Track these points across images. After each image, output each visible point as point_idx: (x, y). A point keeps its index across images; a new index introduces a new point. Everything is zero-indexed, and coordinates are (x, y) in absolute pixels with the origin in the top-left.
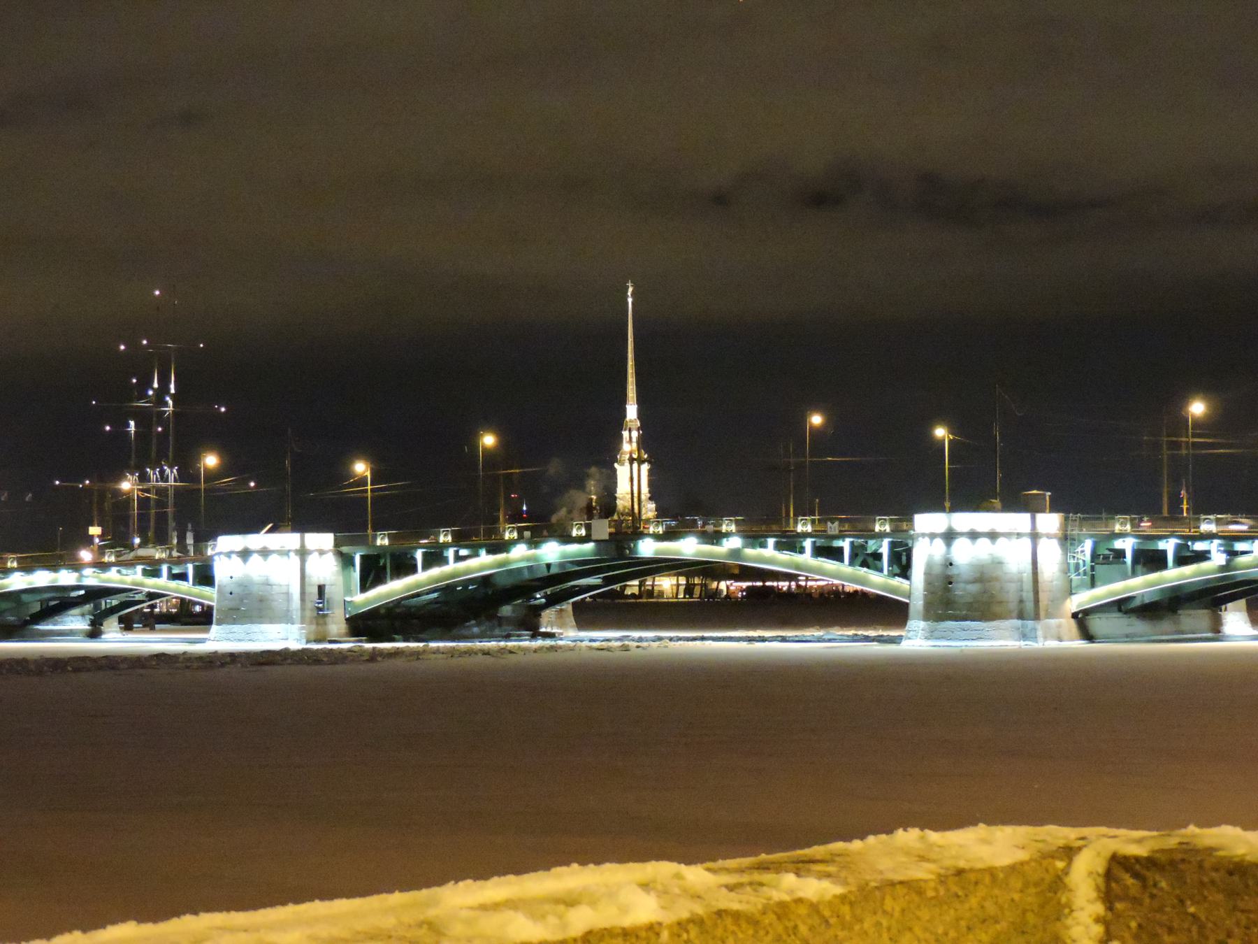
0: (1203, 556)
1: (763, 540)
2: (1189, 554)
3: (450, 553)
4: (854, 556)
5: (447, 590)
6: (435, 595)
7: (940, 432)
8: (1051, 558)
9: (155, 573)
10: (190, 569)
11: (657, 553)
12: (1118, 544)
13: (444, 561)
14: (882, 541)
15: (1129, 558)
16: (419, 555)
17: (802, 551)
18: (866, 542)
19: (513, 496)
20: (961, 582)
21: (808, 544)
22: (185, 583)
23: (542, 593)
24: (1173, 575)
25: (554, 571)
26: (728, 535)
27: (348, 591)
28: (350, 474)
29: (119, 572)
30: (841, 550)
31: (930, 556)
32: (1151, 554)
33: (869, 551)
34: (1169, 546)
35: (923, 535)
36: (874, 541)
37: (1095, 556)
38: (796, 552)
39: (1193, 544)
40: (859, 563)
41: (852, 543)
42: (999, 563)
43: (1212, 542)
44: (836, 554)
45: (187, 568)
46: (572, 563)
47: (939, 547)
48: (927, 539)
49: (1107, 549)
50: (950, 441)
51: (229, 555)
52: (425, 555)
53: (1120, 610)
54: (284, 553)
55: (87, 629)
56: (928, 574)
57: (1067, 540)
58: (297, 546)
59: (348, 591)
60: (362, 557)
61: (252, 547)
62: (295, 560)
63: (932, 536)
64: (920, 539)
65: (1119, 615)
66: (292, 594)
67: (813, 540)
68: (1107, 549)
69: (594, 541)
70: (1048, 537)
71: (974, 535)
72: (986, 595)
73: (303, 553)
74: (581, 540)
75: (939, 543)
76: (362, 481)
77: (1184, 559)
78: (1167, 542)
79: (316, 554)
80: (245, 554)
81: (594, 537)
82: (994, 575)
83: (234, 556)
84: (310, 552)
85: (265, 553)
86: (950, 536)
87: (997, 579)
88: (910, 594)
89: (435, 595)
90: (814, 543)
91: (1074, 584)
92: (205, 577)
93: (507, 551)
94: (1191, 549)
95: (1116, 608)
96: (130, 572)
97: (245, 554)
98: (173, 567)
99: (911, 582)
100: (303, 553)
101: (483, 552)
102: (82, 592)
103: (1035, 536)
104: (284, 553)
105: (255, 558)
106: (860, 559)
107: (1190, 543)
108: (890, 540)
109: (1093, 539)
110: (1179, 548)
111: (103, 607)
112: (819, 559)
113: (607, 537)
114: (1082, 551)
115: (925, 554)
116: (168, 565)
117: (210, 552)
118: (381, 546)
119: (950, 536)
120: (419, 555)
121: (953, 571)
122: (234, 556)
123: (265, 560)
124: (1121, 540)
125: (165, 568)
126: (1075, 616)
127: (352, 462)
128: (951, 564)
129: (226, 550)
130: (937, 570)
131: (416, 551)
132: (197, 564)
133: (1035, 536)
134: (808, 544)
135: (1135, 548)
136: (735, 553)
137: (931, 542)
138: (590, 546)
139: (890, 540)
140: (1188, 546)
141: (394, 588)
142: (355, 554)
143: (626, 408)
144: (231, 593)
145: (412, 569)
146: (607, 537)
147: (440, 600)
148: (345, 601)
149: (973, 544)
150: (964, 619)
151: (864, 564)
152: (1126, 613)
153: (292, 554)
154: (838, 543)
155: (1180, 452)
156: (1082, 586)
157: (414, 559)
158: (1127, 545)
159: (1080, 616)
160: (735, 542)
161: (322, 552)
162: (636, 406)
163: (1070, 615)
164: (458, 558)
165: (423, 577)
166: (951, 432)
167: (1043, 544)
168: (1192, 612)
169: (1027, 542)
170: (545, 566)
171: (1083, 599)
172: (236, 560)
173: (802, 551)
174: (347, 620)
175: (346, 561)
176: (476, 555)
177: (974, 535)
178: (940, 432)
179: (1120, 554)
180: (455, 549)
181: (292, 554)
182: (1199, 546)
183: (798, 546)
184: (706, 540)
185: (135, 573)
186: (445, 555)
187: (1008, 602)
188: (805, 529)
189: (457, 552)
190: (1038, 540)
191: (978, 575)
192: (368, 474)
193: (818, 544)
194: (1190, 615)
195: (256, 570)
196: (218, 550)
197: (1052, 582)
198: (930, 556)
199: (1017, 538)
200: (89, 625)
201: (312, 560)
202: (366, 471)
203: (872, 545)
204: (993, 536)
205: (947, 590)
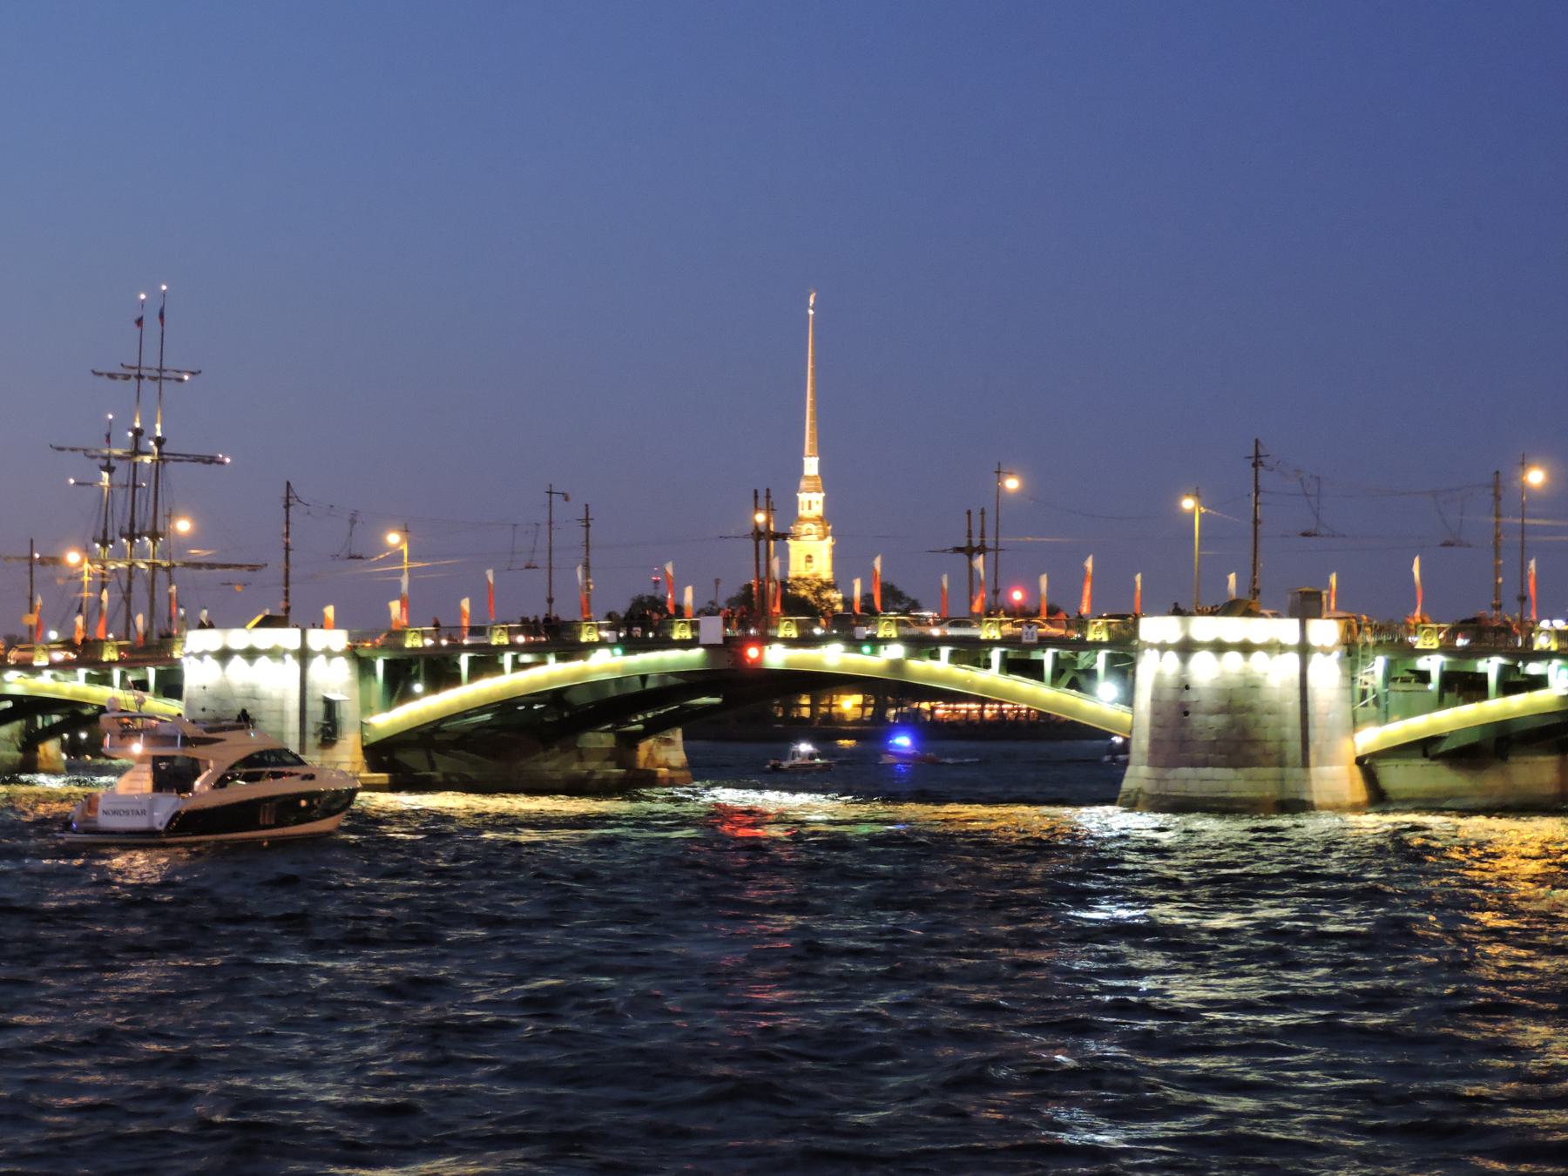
0: (1539, 682)
1: (933, 649)
2: (1519, 679)
3: (507, 659)
4: (1058, 672)
5: (505, 707)
6: (488, 717)
7: (1188, 504)
8: (1327, 677)
9: (105, 680)
10: (151, 673)
11: (788, 663)
12: (1422, 664)
13: (500, 669)
14: (1097, 653)
15: (1434, 685)
16: (464, 660)
17: (987, 665)
18: (1077, 655)
19: (1089, 564)
20: (1199, 712)
21: (996, 655)
22: (109, 689)
23: (640, 717)
24: (1496, 707)
25: (650, 685)
26: (886, 641)
27: (367, 709)
28: (383, 547)
29: (54, 677)
30: (1040, 663)
31: (1159, 676)
32: (1470, 677)
33: (1080, 668)
34: (1490, 667)
35: (1152, 646)
36: (1087, 653)
37: (1389, 678)
38: (979, 666)
39: (1525, 665)
40: (1066, 683)
41: (1056, 656)
42: (1252, 686)
43: (1549, 663)
44: (1032, 670)
45: (147, 674)
46: (672, 674)
47: (1172, 660)
48: (1156, 652)
49: (1407, 670)
50: (1201, 516)
51: (200, 656)
52: (471, 660)
53: (1425, 755)
54: (275, 654)
55: (14, 760)
56: (1155, 700)
57: (1352, 653)
58: (297, 645)
59: (367, 709)
60: (386, 662)
61: (234, 646)
62: (293, 665)
63: (1163, 648)
64: (1147, 651)
65: (1425, 761)
66: (287, 712)
67: (1003, 650)
68: (1407, 670)
69: (704, 646)
70: (1322, 652)
71: (1219, 647)
72: (1235, 731)
73: (304, 655)
74: (685, 644)
75: (1172, 658)
76: (397, 557)
77: (1512, 684)
78: (1489, 662)
79: (322, 658)
80: (224, 655)
81: (702, 641)
82: (1247, 703)
83: (208, 658)
84: (314, 654)
85: (251, 654)
86: (1186, 648)
87: (1250, 709)
88: (1132, 728)
89: (488, 717)
90: (1004, 655)
91: (1359, 718)
92: (171, 686)
93: (585, 658)
94: (1522, 672)
95: (1420, 752)
96: (69, 676)
97: (224, 655)
98: (127, 671)
99: (1133, 710)
100: (304, 655)
101: (551, 659)
102: (9, 704)
103: (1304, 650)
104: (275, 654)
105: (237, 662)
106: (1066, 679)
107: (1520, 664)
108: (1108, 651)
109: (1387, 657)
110: (1504, 671)
111: (40, 725)
112: (1012, 676)
113: (720, 641)
114: (1373, 673)
115: (1153, 669)
116: (122, 669)
117: (176, 655)
118: (413, 649)
119: (1186, 648)
120: (464, 660)
121: (1192, 697)
122: (208, 658)
123: (251, 664)
124: (1425, 657)
125: (116, 673)
126: (1359, 761)
127: (1545, 486)
128: (1187, 687)
129: (198, 650)
130: (1169, 695)
131: (502, 655)
132: (161, 668)
133: (1304, 650)
134: (996, 655)
135: (1445, 669)
136: (896, 666)
137: (1161, 657)
138: (696, 654)
139: (1108, 651)
140: (1518, 669)
141: (426, 705)
142: (376, 658)
143: (802, 462)
144: (204, 710)
145: (453, 680)
146: (720, 641)
147: (495, 723)
148: (362, 723)
149: (1219, 659)
150: (1206, 764)
151: (1073, 684)
152: (1434, 758)
153: (288, 657)
154: (1035, 655)
155: (86, 584)
156: (1369, 720)
157: (458, 666)
158: (1434, 665)
159: (1366, 762)
160: (897, 651)
161: (329, 654)
162: (818, 459)
163: (1353, 760)
164: (518, 666)
165: (471, 692)
166: (1202, 504)
167: (1316, 660)
168: (1529, 759)
169: (1293, 659)
170: (638, 679)
171: (1371, 738)
172: (212, 664)
173: (987, 665)
174: (365, 749)
175: (364, 666)
176: (543, 663)
177: (1219, 647)
178: (1188, 504)
179: (1424, 677)
180: (514, 654)
181: (288, 657)
182: (1534, 669)
183: (982, 657)
184: (851, 648)
185: (76, 679)
186: (501, 662)
187: (1266, 741)
188: (1098, 637)
189: (515, 658)
190: (1308, 655)
191: (1224, 703)
192: (405, 548)
193: (1010, 656)
194: (1527, 763)
195: (239, 674)
196: (187, 650)
197: (1327, 714)
198: (1159, 676)
199: (1280, 653)
200: (19, 750)
201: (317, 667)
202: (401, 543)
203: (1083, 659)
204: (1246, 648)
205: (1183, 724)
